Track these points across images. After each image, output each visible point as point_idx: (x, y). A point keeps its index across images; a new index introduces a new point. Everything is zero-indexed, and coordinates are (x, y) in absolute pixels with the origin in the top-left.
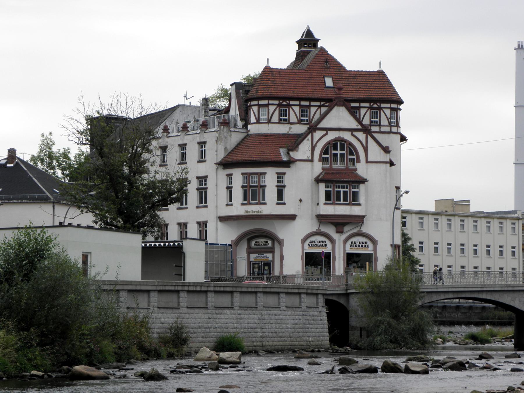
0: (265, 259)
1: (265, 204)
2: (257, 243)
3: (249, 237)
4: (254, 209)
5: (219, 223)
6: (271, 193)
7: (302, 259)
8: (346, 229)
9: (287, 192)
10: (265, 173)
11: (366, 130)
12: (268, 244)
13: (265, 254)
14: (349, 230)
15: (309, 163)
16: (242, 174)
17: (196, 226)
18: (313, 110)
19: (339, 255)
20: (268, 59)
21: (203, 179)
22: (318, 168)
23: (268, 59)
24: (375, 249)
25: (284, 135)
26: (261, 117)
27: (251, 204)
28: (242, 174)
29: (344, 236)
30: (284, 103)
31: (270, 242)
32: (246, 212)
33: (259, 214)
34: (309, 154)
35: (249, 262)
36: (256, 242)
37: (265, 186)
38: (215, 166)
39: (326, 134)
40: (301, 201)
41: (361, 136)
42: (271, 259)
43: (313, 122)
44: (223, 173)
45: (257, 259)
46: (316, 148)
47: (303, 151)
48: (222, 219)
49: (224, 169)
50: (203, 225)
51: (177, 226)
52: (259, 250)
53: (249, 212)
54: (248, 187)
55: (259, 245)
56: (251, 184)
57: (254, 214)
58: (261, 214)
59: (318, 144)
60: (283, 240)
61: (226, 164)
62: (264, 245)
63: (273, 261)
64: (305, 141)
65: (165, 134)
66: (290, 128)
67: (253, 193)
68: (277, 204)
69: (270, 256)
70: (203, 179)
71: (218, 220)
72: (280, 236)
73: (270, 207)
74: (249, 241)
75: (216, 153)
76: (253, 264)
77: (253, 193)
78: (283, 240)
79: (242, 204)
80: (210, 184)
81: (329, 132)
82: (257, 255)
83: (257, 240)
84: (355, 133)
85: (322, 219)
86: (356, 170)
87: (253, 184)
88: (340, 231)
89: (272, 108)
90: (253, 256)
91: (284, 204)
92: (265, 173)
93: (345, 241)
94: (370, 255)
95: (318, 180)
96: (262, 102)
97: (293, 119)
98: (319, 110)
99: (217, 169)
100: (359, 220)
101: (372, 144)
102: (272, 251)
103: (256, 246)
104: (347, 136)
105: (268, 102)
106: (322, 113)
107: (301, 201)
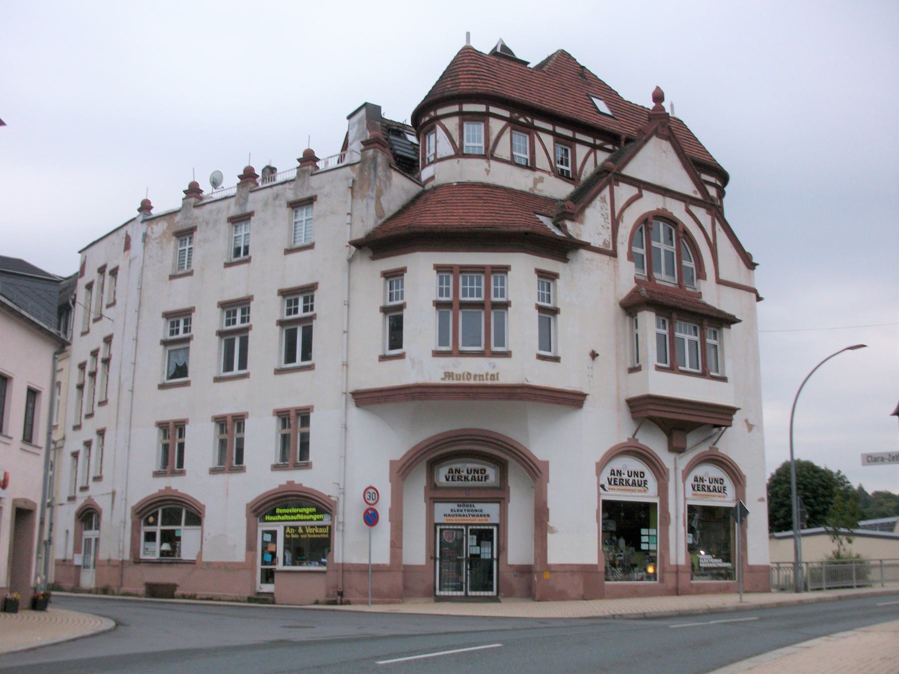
0: (477, 520)
1: (507, 354)
2: (454, 474)
3: (432, 457)
4: (473, 369)
5: (354, 412)
6: (521, 326)
7: (598, 522)
8: (691, 439)
9: (562, 325)
10: (505, 269)
11: (714, 205)
12: (486, 478)
13: (478, 506)
14: (696, 447)
15: (606, 258)
16: (439, 269)
17: (272, 425)
18: (581, 151)
19: (677, 510)
20: (468, 34)
21: (299, 296)
22: (626, 276)
23: (468, 34)
24: (663, 491)
25: (522, 193)
26: (466, 144)
27: (463, 354)
28: (439, 269)
29: (685, 460)
30: (522, 120)
31: (492, 474)
32: (448, 375)
33: (489, 382)
34: (607, 235)
35: (433, 527)
36: (451, 471)
37: (506, 305)
38: (348, 251)
39: (639, 196)
40: (594, 355)
41: (701, 214)
42: (495, 519)
43: (583, 178)
44: (370, 273)
45: (455, 520)
46: (621, 226)
47: (592, 226)
48: (365, 399)
49: (374, 258)
50: (295, 425)
51: (213, 424)
52: (462, 495)
53: (458, 377)
54: (456, 306)
55: (459, 479)
56: (461, 298)
57: (472, 382)
58: (496, 382)
59: (626, 214)
60: (546, 463)
61: (380, 244)
62: (473, 479)
63: (501, 526)
64: (597, 202)
65: (193, 200)
66: (537, 181)
67: (472, 315)
68: (541, 357)
69: (491, 511)
70: (299, 296)
71: (352, 403)
72: (539, 450)
73: (520, 367)
74: (433, 465)
75: (348, 219)
76: (441, 530)
77: (472, 315)
78: (546, 463)
79: (437, 354)
80: (324, 305)
81: (645, 192)
82: (454, 506)
83: (454, 467)
84: (693, 209)
85: (647, 411)
86: (700, 295)
87: (468, 299)
88: (677, 449)
89: (496, 125)
90: (442, 511)
91: (556, 359)
92: (505, 269)
93: (686, 474)
94: (647, 508)
95: (631, 307)
96: (468, 108)
97: (542, 161)
98: (592, 155)
99: (350, 261)
100: (722, 416)
101: (722, 239)
102: (499, 496)
103: (451, 483)
104: (677, 209)
105: (488, 109)
106: (599, 162)
107: (594, 355)
